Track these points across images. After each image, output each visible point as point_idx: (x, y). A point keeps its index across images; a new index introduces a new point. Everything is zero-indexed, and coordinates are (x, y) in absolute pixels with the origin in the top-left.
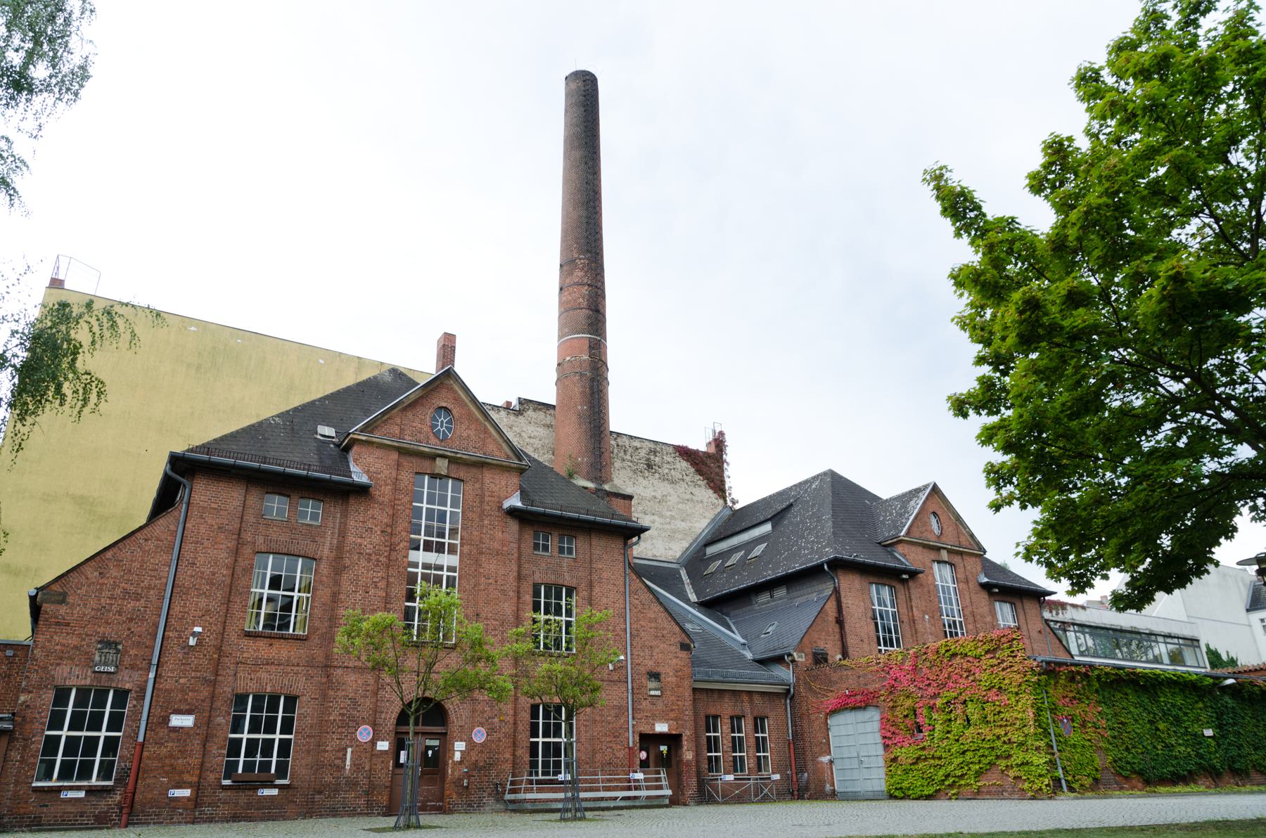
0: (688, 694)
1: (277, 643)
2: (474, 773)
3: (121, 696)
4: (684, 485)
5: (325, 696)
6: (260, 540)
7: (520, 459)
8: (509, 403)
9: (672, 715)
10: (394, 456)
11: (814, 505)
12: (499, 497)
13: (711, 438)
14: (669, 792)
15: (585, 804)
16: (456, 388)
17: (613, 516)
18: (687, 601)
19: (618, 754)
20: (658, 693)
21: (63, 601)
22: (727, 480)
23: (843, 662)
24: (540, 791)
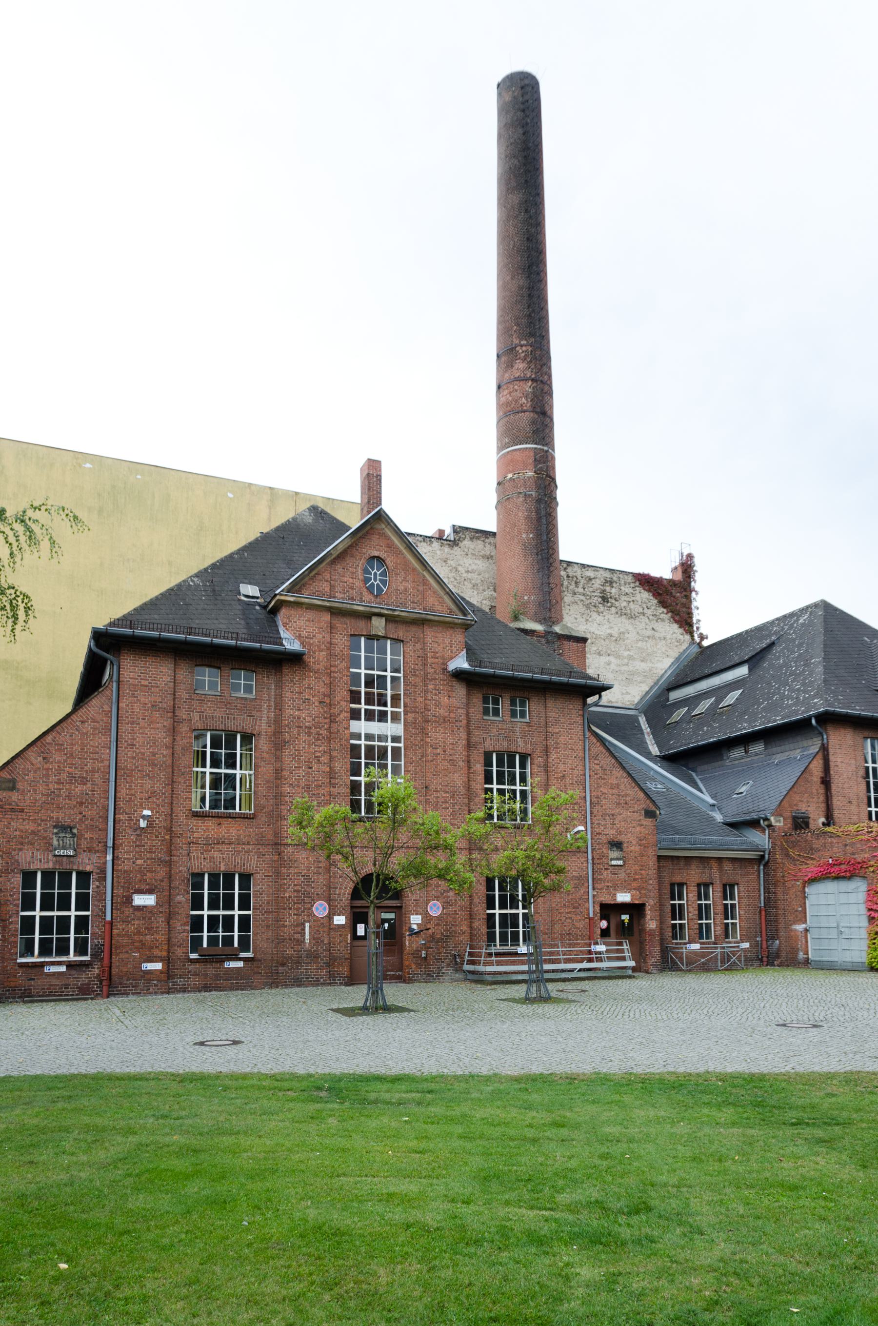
0: (652, 863)
1: (225, 823)
2: (432, 945)
3: (84, 878)
4: (644, 620)
5: (278, 874)
6: (196, 716)
7: (464, 613)
8: (441, 532)
9: (635, 884)
10: (327, 617)
11: (800, 645)
12: (443, 658)
13: (676, 562)
14: (632, 964)
15: (547, 976)
16: (389, 532)
17: (571, 674)
18: (648, 754)
19: (577, 925)
20: (620, 863)
21: (13, 788)
22: (695, 612)
23: (828, 829)
24: (499, 963)
